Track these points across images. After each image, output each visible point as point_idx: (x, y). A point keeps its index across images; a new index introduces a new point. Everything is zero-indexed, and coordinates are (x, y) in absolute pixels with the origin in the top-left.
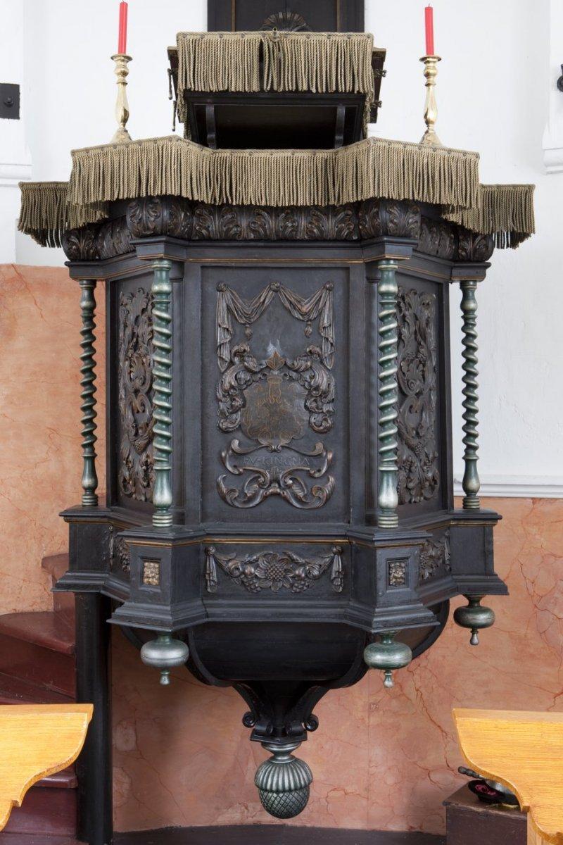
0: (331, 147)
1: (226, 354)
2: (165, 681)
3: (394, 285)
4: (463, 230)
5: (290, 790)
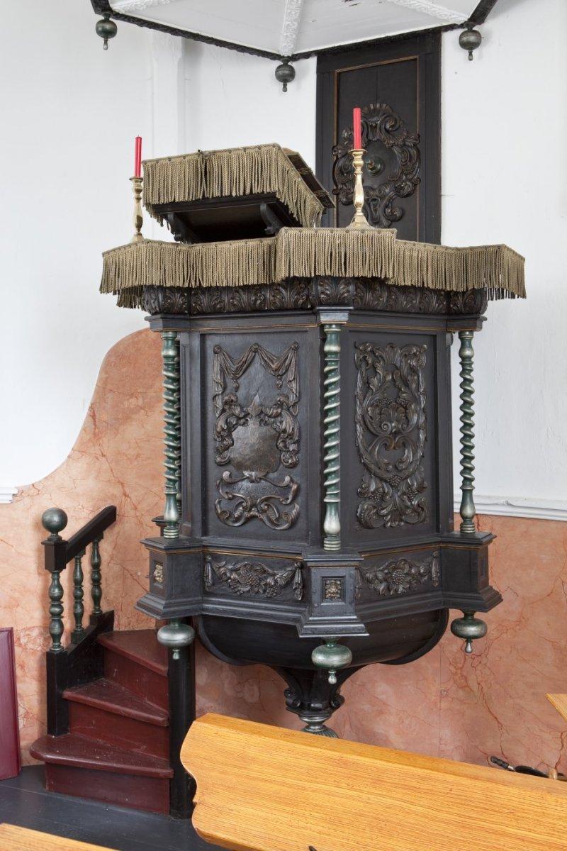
3: (335, 345)
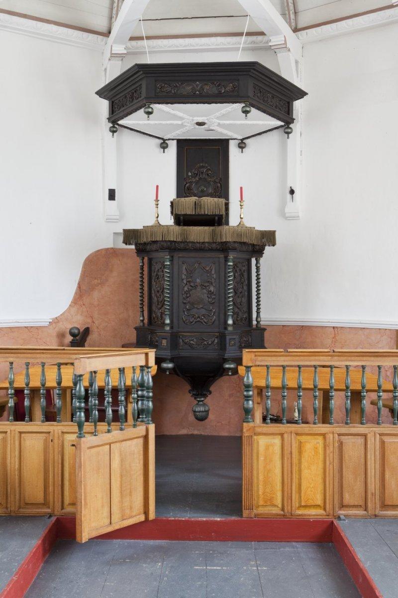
1: (185, 282)
2: (168, 373)
4: (257, 244)
5: (203, 412)
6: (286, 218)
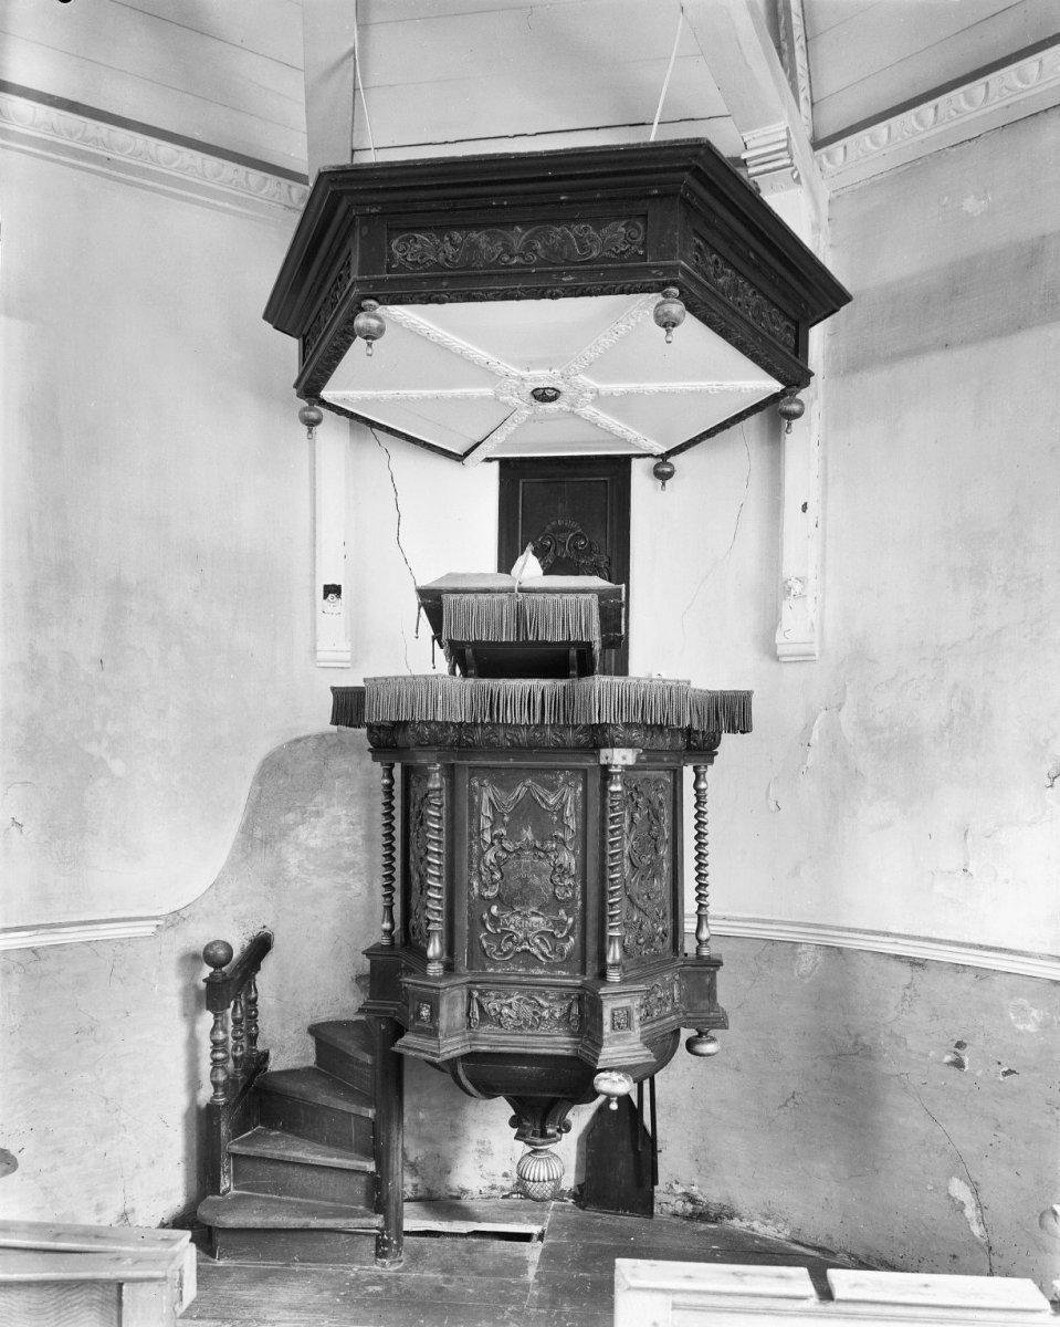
0: (567, 677)
1: (487, 837)
6: (776, 658)
